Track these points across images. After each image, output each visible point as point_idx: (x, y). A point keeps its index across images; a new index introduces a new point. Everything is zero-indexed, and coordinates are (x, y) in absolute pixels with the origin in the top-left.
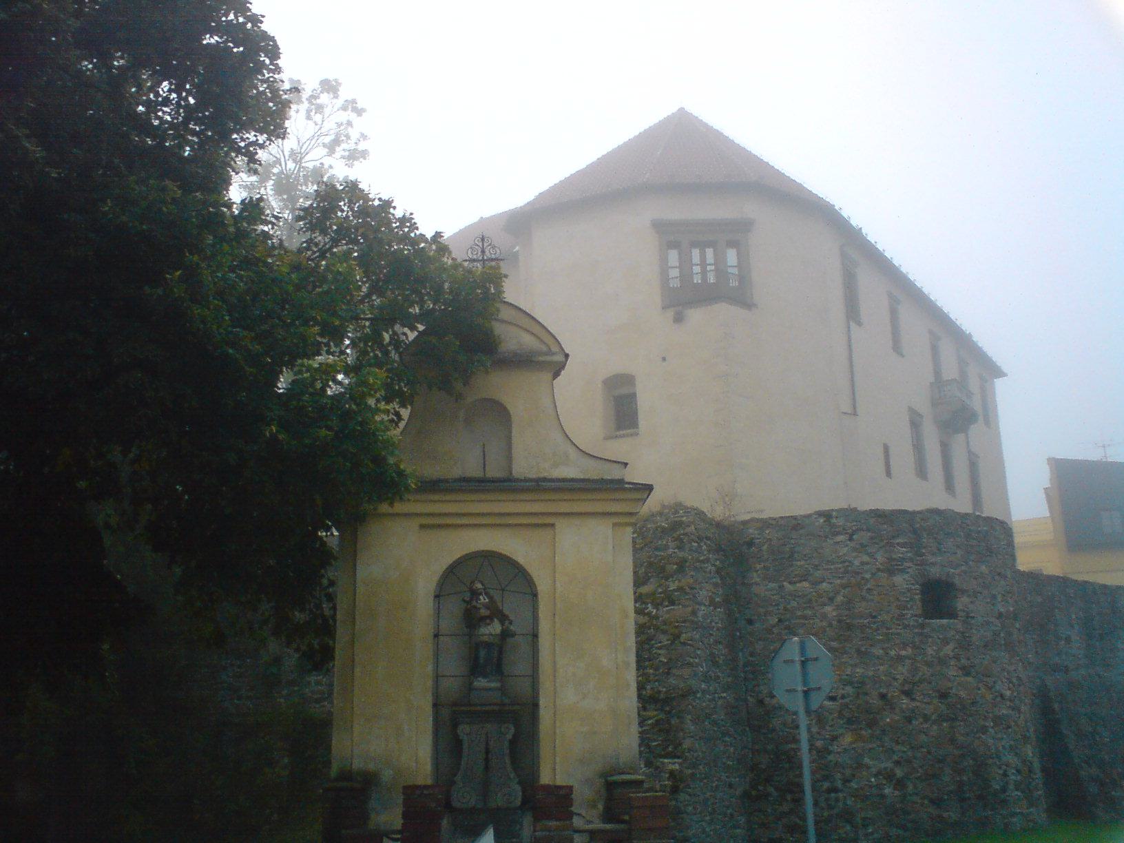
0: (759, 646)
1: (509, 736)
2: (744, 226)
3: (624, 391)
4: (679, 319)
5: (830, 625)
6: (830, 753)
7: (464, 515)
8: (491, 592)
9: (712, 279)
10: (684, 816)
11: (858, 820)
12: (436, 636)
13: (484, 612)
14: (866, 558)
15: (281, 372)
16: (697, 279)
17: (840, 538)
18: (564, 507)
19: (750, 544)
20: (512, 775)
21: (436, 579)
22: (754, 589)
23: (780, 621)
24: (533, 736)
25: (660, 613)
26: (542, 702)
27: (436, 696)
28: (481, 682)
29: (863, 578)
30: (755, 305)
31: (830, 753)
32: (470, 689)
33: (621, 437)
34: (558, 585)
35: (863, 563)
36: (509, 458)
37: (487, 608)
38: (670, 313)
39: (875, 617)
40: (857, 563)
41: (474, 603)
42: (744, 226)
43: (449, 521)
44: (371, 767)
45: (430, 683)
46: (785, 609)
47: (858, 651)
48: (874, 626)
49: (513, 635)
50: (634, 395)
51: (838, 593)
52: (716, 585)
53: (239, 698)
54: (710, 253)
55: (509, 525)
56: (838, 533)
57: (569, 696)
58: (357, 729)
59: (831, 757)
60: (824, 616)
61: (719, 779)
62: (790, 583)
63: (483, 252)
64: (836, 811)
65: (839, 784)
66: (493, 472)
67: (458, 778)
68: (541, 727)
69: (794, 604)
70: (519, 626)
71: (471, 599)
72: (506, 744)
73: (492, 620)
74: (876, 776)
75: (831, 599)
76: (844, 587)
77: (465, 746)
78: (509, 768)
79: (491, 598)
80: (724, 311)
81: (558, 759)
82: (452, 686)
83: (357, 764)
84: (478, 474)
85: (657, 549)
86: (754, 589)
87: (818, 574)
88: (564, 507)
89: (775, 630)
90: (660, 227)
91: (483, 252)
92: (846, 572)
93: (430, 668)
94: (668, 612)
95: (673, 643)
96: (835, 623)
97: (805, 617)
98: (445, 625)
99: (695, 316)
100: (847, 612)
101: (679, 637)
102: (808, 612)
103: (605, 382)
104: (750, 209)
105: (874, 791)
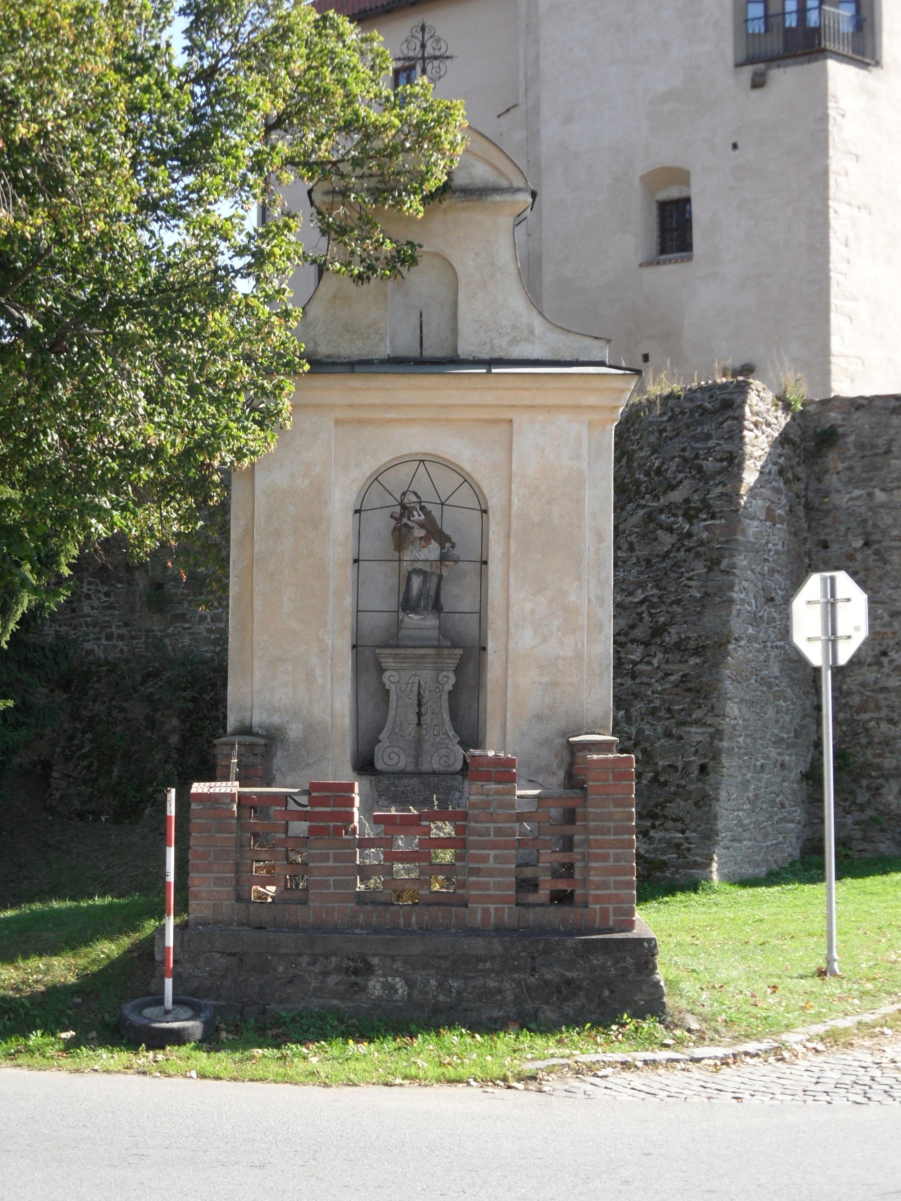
1: (449, 687)
3: (673, 193)
4: (758, 83)
7: (391, 407)
8: (429, 507)
12: (356, 561)
16: (791, 21)
18: (526, 397)
20: (452, 733)
21: (355, 489)
23: (866, 544)
24: (478, 686)
25: (695, 529)
26: (491, 645)
27: (357, 633)
28: (413, 619)
32: (399, 623)
33: (665, 262)
34: (515, 499)
36: (455, 331)
37: (422, 526)
41: (405, 520)
43: (374, 415)
44: (276, 720)
45: (348, 620)
50: (687, 201)
52: (778, 491)
53: (109, 637)
55: (449, 421)
57: (525, 639)
58: (258, 675)
61: (767, 757)
62: (884, 490)
63: (423, 46)
66: (432, 350)
67: (383, 736)
68: (489, 675)
69: (889, 520)
70: (466, 549)
71: (402, 515)
72: (445, 696)
77: (393, 697)
78: (448, 726)
79: (428, 514)
81: (509, 715)
82: (377, 623)
83: (258, 718)
84: (414, 352)
85: (694, 438)
88: (526, 397)
89: (859, 556)
91: (423, 46)
93: (348, 601)
94: (706, 528)
95: (710, 570)
98: (369, 548)
101: (719, 563)
103: (643, 179)
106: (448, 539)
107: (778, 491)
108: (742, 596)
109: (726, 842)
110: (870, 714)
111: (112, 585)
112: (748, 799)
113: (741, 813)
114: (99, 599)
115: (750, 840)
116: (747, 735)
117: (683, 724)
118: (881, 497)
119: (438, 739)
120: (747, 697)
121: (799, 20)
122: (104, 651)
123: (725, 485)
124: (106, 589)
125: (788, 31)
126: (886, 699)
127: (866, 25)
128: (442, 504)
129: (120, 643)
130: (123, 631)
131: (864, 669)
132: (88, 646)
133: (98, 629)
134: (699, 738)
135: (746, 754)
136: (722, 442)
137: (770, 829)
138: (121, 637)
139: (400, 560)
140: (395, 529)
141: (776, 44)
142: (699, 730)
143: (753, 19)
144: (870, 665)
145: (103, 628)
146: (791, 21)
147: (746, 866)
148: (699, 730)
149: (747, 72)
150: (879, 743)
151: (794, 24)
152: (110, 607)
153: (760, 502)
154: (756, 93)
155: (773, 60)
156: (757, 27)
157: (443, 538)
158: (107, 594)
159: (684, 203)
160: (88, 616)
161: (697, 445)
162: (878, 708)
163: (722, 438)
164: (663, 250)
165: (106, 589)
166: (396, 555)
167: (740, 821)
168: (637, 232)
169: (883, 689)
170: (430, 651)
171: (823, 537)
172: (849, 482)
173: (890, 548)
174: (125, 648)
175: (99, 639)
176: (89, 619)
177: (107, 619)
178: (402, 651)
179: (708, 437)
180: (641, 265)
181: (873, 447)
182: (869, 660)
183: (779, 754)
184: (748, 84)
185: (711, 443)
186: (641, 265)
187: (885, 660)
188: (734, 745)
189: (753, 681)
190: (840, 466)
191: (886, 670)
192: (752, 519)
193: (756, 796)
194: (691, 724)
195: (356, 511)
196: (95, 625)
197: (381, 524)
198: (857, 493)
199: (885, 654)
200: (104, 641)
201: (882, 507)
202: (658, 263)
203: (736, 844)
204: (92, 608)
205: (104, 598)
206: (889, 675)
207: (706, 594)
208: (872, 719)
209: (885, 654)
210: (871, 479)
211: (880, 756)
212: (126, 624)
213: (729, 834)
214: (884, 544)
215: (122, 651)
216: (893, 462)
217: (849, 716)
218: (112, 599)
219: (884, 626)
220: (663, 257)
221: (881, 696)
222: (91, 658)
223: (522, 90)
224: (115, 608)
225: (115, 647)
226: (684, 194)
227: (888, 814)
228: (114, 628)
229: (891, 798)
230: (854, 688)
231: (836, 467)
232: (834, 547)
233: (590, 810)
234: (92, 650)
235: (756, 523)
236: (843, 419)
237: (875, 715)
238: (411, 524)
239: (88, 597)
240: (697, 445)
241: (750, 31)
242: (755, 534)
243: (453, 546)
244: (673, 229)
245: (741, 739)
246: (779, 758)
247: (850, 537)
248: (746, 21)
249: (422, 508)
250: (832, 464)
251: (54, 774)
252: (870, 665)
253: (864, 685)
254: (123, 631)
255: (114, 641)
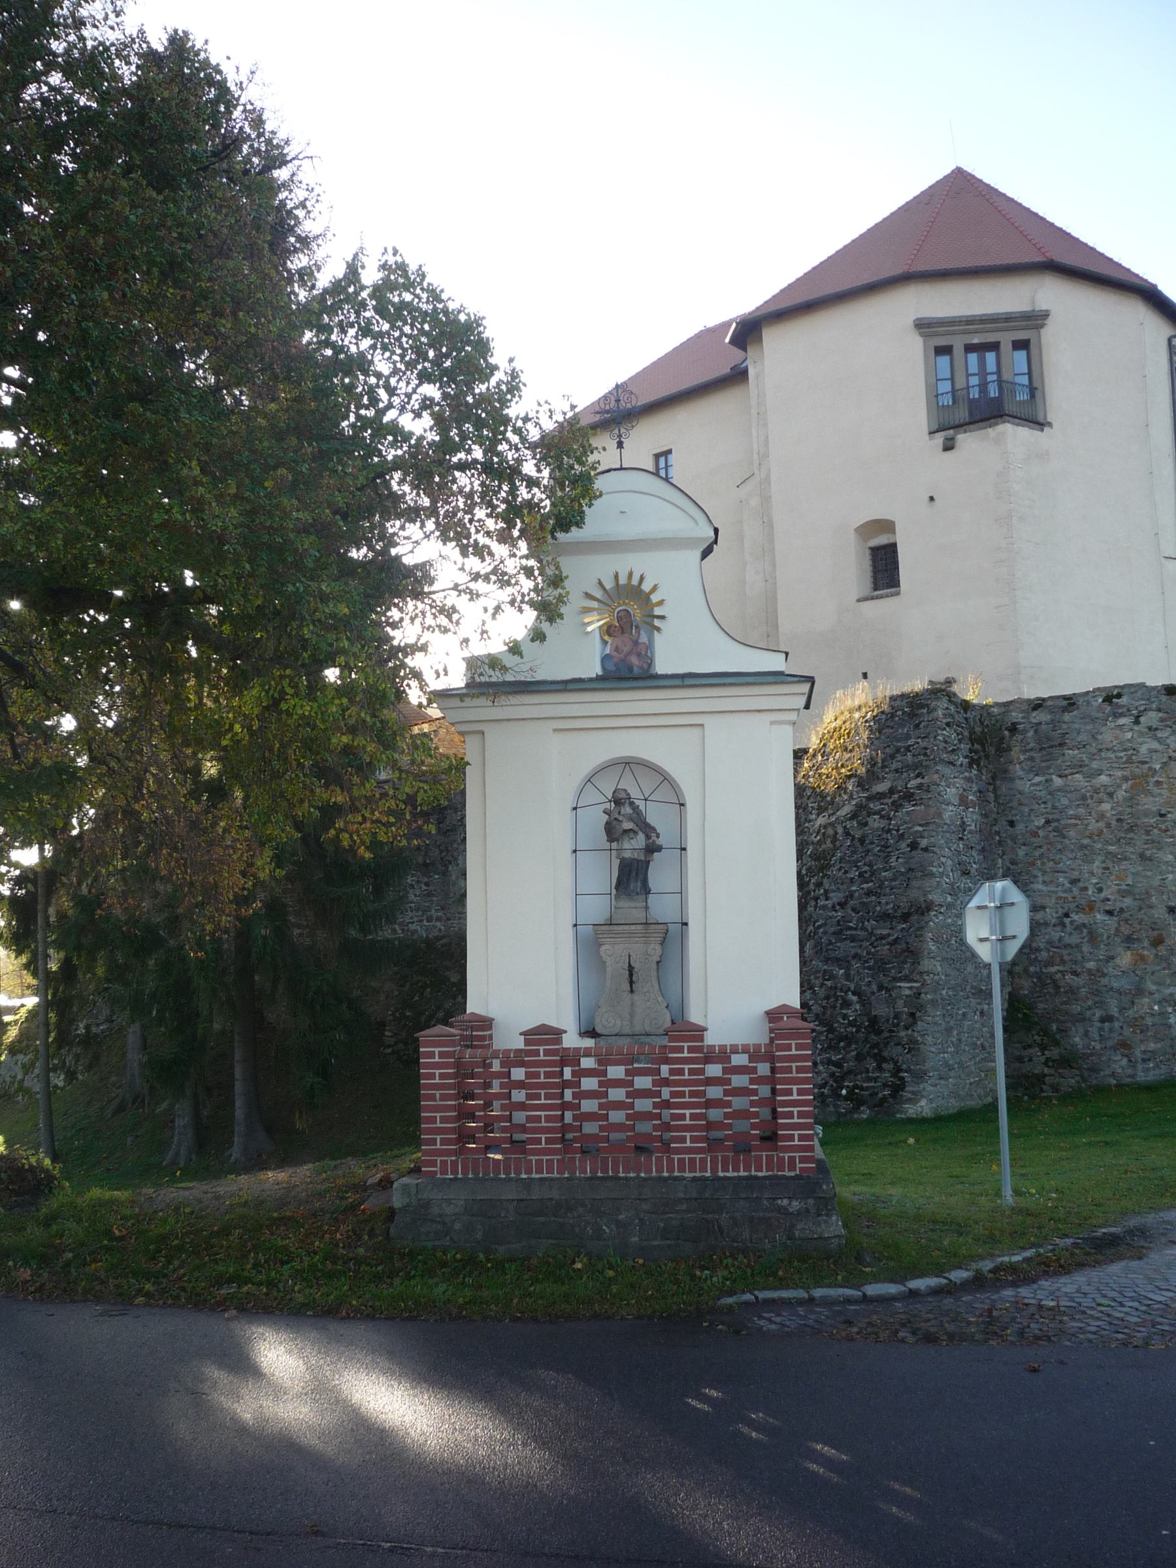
0: (1021, 852)
2: (1036, 319)
3: (882, 540)
4: (949, 446)
5: (1108, 825)
6: (1104, 975)
8: (637, 802)
9: (993, 392)
10: (922, 1046)
11: (1138, 1054)
13: (627, 825)
14: (1155, 745)
15: (398, 558)
16: (975, 394)
17: (1122, 721)
19: (1013, 729)
22: (1019, 784)
23: (1048, 822)
29: (1150, 769)
30: (1050, 424)
31: (1104, 975)
35: (1151, 751)
38: (939, 438)
39: (1162, 815)
40: (1144, 749)
42: (1036, 319)
46: (1054, 807)
47: (1142, 856)
48: (1059, 847)
49: (659, 849)
50: (894, 545)
51: (1119, 786)
53: (429, 920)
54: (990, 357)
56: (1122, 715)
59: (1105, 981)
60: (1101, 816)
62: (1060, 776)
64: (1110, 1043)
65: (1114, 1011)
69: (1065, 801)
73: (635, 833)
74: (1159, 1003)
75: (1111, 795)
76: (1126, 779)
80: (1013, 434)
86: (1019, 784)
87: (1095, 765)
89: (1041, 833)
90: (923, 326)
91: (618, 401)
92: (1129, 761)
96: (1114, 823)
97: (1077, 817)
99: (966, 440)
100: (1129, 810)
102: (1082, 811)
104: (1048, 294)
105: (1157, 1019)
106: (654, 829)
107: (969, 780)
110: (1056, 968)
117: (895, 979)
118: (1058, 782)
121: (980, 392)
124: (426, 879)
125: (971, 402)
126: (1069, 954)
127: (1038, 394)
131: (1050, 929)
134: (908, 992)
137: (973, 1068)
138: (439, 919)
141: (962, 414)
144: (1054, 925)
145: (424, 911)
146: (975, 394)
147: (952, 1100)
148: (907, 985)
149: (939, 438)
150: (1066, 992)
151: (977, 396)
152: (430, 894)
153: (954, 790)
154: (948, 453)
155: (959, 427)
156: (947, 400)
158: (427, 884)
159: (892, 548)
162: (1063, 962)
165: (426, 879)
168: (854, 569)
169: (1066, 946)
171: (1010, 818)
172: (1030, 771)
173: (1066, 826)
175: (421, 921)
178: (615, 928)
179: (908, 737)
180: (858, 601)
181: (1049, 739)
182: (1054, 921)
183: (979, 1004)
186: (858, 601)
187: (1067, 921)
188: (938, 997)
190: (1022, 758)
191: (1069, 929)
192: (948, 805)
193: (960, 1040)
195: (575, 809)
196: (417, 910)
197: (595, 818)
198: (1037, 779)
199: (1067, 915)
200: (425, 923)
201: (1059, 790)
202: (872, 598)
203: (943, 1082)
205: (424, 887)
206: (1071, 934)
208: (1059, 971)
209: (1067, 915)
210: (1049, 768)
211: (1066, 1003)
212: (443, 908)
214: (1062, 822)
216: (1067, 752)
217: (1038, 969)
218: (431, 888)
219: (1065, 891)
221: (1065, 952)
222: (415, 937)
225: (435, 927)
227: (989, 1053)
228: (433, 912)
229: (1077, 1039)
230: (1042, 946)
231: (1018, 758)
232: (1020, 827)
234: (416, 931)
235: (951, 808)
236: (1023, 718)
237: (1061, 968)
238: (621, 818)
239: (412, 886)
242: (950, 817)
243: (658, 836)
244: (884, 567)
245: (944, 992)
246: (979, 1007)
247: (1032, 817)
248: (937, 396)
249: (632, 804)
250: (1016, 756)
252: (1054, 925)
253: (1050, 942)
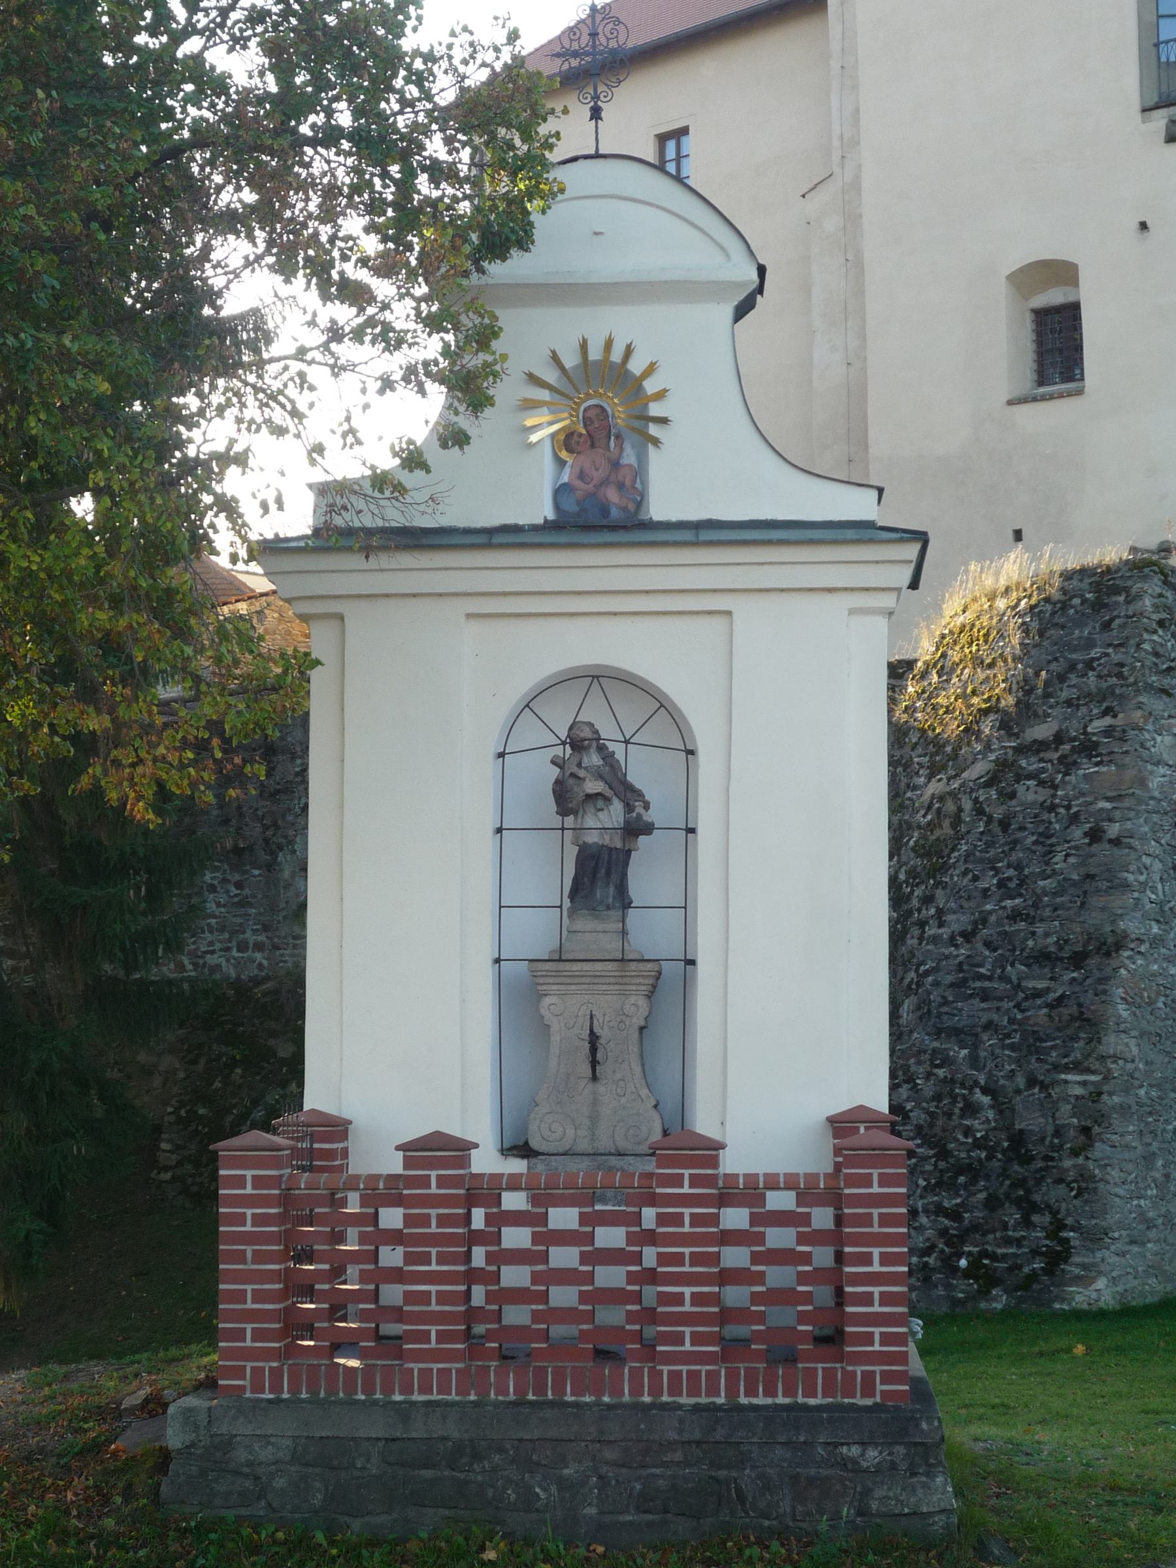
3: (1055, 297)
8: (611, 746)
53: (243, 947)
106: (639, 794)
108: (1142, 878)
109: (1118, 1246)
111: (247, 872)
112: (1154, 1180)
113: (1142, 1202)
114: (228, 892)
115: (1158, 1241)
116: (1151, 1085)
117: (1057, 1068)
119: (623, 1100)
120: (1152, 1029)
122: (235, 967)
123: (1115, 716)
124: (237, 877)
128: (627, 742)
129: (258, 956)
130: (261, 938)
132: (212, 960)
133: (226, 935)
135: (1150, 1113)
136: (1110, 650)
138: (259, 947)
139: (563, 829)
140: (558, 783)
142: (1078, 1078)
143: (1167, 42)
145: (233, 933)
148: (1078, 1078)
157: (629, 794)
158: (239, 885)
159: (1073, 310)
160: (213, 916)
161: (1074, 656)
163: (1109, 645)
164: (1042, 381)
165: (237, 877)
166: (557, 821)
167: (1142, 1214)
170: (610, 966)
174: (265, 962)
175: (228, 949)
176: (213, 921)
177: (239, 920)
179: (1090, 644)
180: (1010, 403)
184: (1162, 135)
185: (1095, 653)
186: (1010, 403)
189: (1161, 1005)
194: (1066, 1069)
195: (501, 755)
196: (222, 929)
200: (235, 953)
202: (1035, 399)
203: (1135, 1249)
204: (218, 905)
205: (234, 891)
207: (1090, 877)
212: (266, 928)
213: (1124, 1233)
215: (260, 965)
218: (247, 891)
220: (1042, 390)
223: (836, 157)
224: (251, 905)
226: (1071, 299)
228: (248, 934)
233: (846, 1211)
234: (219, 966)
239: (213, 889)
240: (1074, 656)
241: (1163, 59)
244: (1057, 345)
245: (1142, 1092)
248: (1157, 45)
249: (601, 749)
251: (164, 1146)
254: (261, 938)
255: (249, 953)
